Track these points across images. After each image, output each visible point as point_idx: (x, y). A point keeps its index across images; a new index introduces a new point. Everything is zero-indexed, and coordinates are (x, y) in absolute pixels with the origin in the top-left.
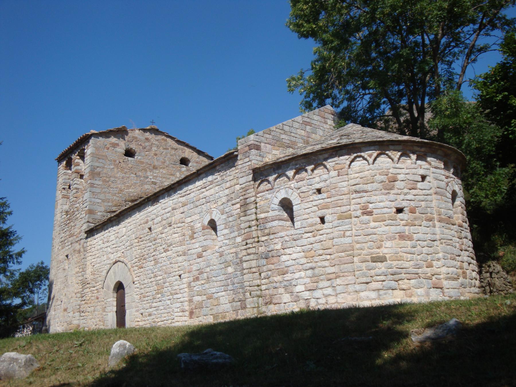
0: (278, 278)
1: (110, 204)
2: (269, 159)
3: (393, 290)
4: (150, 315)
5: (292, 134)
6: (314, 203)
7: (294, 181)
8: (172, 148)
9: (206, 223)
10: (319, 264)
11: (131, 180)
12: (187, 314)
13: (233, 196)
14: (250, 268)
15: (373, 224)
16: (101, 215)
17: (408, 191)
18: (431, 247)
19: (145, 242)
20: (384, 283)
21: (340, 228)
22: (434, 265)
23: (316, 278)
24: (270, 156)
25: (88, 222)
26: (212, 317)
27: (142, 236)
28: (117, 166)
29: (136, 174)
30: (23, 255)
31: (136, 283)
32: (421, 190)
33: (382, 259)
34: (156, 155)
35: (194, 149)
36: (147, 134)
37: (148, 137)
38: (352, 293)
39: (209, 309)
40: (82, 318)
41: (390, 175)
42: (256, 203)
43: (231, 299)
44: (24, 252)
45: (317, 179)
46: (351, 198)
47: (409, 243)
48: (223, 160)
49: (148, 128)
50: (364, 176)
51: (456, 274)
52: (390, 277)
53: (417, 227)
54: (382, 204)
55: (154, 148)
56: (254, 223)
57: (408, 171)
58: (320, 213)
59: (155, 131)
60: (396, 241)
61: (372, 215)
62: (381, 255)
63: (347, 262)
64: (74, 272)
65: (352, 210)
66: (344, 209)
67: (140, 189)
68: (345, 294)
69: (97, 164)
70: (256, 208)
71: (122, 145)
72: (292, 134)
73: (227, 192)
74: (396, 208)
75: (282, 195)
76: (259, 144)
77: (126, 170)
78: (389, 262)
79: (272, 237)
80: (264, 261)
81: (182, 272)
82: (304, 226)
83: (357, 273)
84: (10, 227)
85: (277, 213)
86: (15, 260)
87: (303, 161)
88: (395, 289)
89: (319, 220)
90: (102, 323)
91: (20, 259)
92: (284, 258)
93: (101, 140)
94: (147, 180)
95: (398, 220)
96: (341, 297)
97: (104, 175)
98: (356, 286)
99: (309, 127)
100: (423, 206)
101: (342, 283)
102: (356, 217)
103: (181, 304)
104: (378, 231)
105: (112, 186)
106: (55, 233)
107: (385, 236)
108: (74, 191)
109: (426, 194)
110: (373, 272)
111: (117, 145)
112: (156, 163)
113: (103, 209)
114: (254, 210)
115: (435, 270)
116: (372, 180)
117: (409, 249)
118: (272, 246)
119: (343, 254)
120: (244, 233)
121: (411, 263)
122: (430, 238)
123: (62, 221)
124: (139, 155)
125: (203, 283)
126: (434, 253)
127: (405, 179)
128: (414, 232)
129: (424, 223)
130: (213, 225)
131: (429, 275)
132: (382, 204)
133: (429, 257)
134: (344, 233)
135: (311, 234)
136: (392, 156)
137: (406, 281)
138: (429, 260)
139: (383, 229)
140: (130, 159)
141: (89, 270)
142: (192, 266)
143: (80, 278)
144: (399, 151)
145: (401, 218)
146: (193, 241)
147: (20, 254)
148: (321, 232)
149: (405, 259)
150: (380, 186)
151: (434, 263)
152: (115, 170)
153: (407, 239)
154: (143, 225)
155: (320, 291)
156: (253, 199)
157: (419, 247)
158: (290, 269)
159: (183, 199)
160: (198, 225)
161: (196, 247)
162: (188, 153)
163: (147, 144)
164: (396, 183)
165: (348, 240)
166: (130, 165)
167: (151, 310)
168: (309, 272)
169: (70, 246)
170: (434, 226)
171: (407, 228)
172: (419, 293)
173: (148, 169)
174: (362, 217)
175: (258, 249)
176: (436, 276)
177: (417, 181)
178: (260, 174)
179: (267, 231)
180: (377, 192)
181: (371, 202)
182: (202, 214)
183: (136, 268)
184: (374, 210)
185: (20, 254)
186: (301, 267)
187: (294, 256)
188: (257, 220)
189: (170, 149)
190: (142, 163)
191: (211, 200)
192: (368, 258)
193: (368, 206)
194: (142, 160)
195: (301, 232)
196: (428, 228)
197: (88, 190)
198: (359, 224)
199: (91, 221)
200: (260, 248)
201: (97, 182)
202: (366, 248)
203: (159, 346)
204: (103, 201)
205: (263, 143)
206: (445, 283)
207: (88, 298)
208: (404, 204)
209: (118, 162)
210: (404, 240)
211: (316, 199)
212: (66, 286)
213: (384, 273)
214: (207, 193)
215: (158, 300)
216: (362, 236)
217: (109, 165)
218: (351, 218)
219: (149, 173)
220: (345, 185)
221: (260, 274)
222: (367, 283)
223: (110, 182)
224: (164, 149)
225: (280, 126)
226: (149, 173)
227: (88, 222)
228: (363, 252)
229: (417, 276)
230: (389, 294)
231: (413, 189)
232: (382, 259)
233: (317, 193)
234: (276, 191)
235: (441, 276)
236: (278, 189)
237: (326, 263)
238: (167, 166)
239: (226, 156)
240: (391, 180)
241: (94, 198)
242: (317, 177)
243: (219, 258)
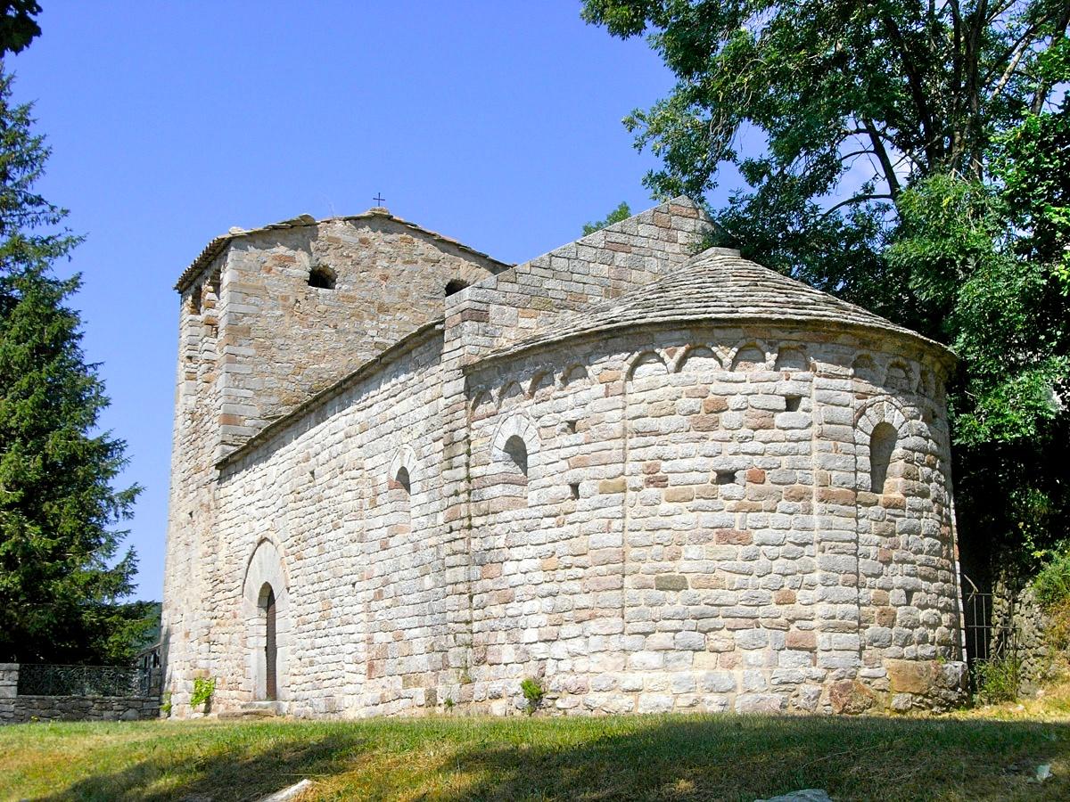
0: (497, 610)
1: (274, 400)
2: (508, 341)
3: (694, 650)
4: (312, 664)
5: (576, 277)
6: (563, 453)
7: (531, 401)
8: (427, 260)
9: (394, 475)
10: (564, 586)
11: (325, 341)
12: (363, 668)
13: (434, 420)
14: (456, 583)
15: (665, 507)
16: (250, 427)
17: (749, 432)
18: (794, 559)
19: (305, 503)
20: (678, 636)
21: (603, 512)
22: (798, 598)
23: (557, 616)
24: (512, 334)
25: (223, 442)
26: (400, 678)
27: (300, 489)
28: (290, 310)
29: (335, 327)
30: (137, 497)
31: (291, 590)
32: (784, 429)
33: (677, 585)
34: (385, 278)
35: (481, 259)
36: (366, 232)
37: (367, 236)
38: (615, 654)
39: (397, 661)
40: (212, 655)
41: (711, 397)
42: (469, 443)
43: (428, 645)
44: (137, 491)
45: (570, 400)
46: (628, 446)
47: (740, 549)
48: (419, 339)
49: (366, 214)
50: (655, 398)
51: (855, 618)
52: (691, 623)
53: (763, 513)
54: (687, 463)
55: (382, 263)
56: (463, 486)
57: (753, 387)
58: (571, 475)
59: (383, 222)
60: (710, 544)
61: (666, 486)
62: (677, 574)
63: (610, 586)
64: (200, 554)
65: (627, 473)
66: (613, 470)
67: (345, 362)
68: (604, 655)
69: (242, 309)
70: (469, 453)
71: (303, 264)
72: (576, 277)
73: (426, 410)
74: (717, 471)
75: (509, 430)
76: (483, 307)
77: (311, 319)
78: (690, 589)
79: (491, 519)
80: (476, 571)
81: (355, 578)
82: (542, 501)
83: (628, 611)
84: (106, 435)
85: (500, 468)
86: (120, 509)
87: (548, 357)
88: (700, 650)
89: (568, 489)
90: (241, 672)
91: (131, 507)
92: (509, 567)
93: (253, 253)
94: (364, 339)
95: (720, 499)
96: (595, 660)
97: (260, 333)
98: (624, 638)
99: (624, 255)
100: (784, 466)
101: (599, 632)
102: (634, 489)
103: (355, 645)
104: (674, 521)
105: (278, 358)
106: (174, 460)
107: (687, 534)
108: (204, 367)
109: (794, 438)
110: (656, 612)
111: (292, 260)
112: (386, 299)
113: (257, 412)
114: (464, 458)
115: (798, 609)
116: (669, 409)
117: (740, 564)
118: (491, 539)
119: (604, 568)
120: (448, 507)
121: (741, 593)
122: (792, 540)
123: (185, 432)
124: (345, 282)
125: (388, 604)
126: (800, 571)
127: (744, 405)
128: (754, 524)
129: (784, 504)
130: (403, 479)
131: (782, 620)
132: (687, 463)
133: (787, 581)
134: (610, 523)
135: (553, 519)
136: (720, 354)
137: (724, 632)
138: (786, 588)
139: (685, 517)
140: (322, 291)
141: (223, 552)
142: (373, 566)
143: (210, 568)
144: (732, 347)
145: (727, 493)
146: (375, 512)
147: (130, 496)
148: (571, 518)
149: (727, 586)
150: (685, 421)
151: (799, 594)
152: (287, 319)
153: (735, 541)
154: (303, 464)
155: (561, 644)
156: (463, 432)
157: (763, 559)
158: (518, 591)
159: (361, 416)
160: (383, 478)
161: (378, 523)
162: (465, 269)
163: (364, 253)
164: (723, 414)
165: (615, 539)
166: (322, 307)
167: (312, 653)
168: (548, 601)
169: (195, 493)
170: (809, 512)
171: (738, 516)
172: (751, 661)
173: (365, 314)
174: (646, 489)
175: (469, 543)
176: (798, 623)
177: (776, 411)
178: (487, 379)
179: (483, 506)
180: (678, 436)
181: (664, 457)
182: (390, 453)
183: (292, 558)
184: (669, 475)
185: (130, 496)
186: (533, 590)
187: (525, 565)
188: (469, 479)
189: (420, 261)
190: (352, 299)
191: (403, 424)
192: (651, 579)
193: (659, 466)
194: (352, 293)
195: (537, 514)
196: (793, 517)
197: (224, 369)
198: (638, 506)
199: (229, 439)
200: (473, 541)
201: (243, 351)
202: (649, 558)
203: (209, 756)
204: (258, 393)
205: (495, 303)
206: (821, 639)
207: (221, 614)
208: (737, 462)
209: (292, 300)
210: (729, 542)
211: (567, 444)
212: (189, 582)
213: (678, 613)
214: (398, 409)
215: (324, 632)
216: (643, 533)
217: (272, 309)
218: (624, 491)
219: (367, 324)
220: (616, 418)
221: (471, 598)
222: (646, 634)
223: (274, 349)
224: (407, 262)
225: (542, 260)
226: (367, 324)
227: (223, 442)
228: (643, 566)
229: (751, 621)
230: (686, 660)
231: (761, 428)
232: (677, 585)
233: (569, 430)
234: (502, 420)
235: (815, 624)
236: (504, 416)
237: (576, 586)
238: (412, 305)
239: (421, 332)
240: (710, 409)
241: (238, 387)
242: (584, 395)
243: (413, 555)
